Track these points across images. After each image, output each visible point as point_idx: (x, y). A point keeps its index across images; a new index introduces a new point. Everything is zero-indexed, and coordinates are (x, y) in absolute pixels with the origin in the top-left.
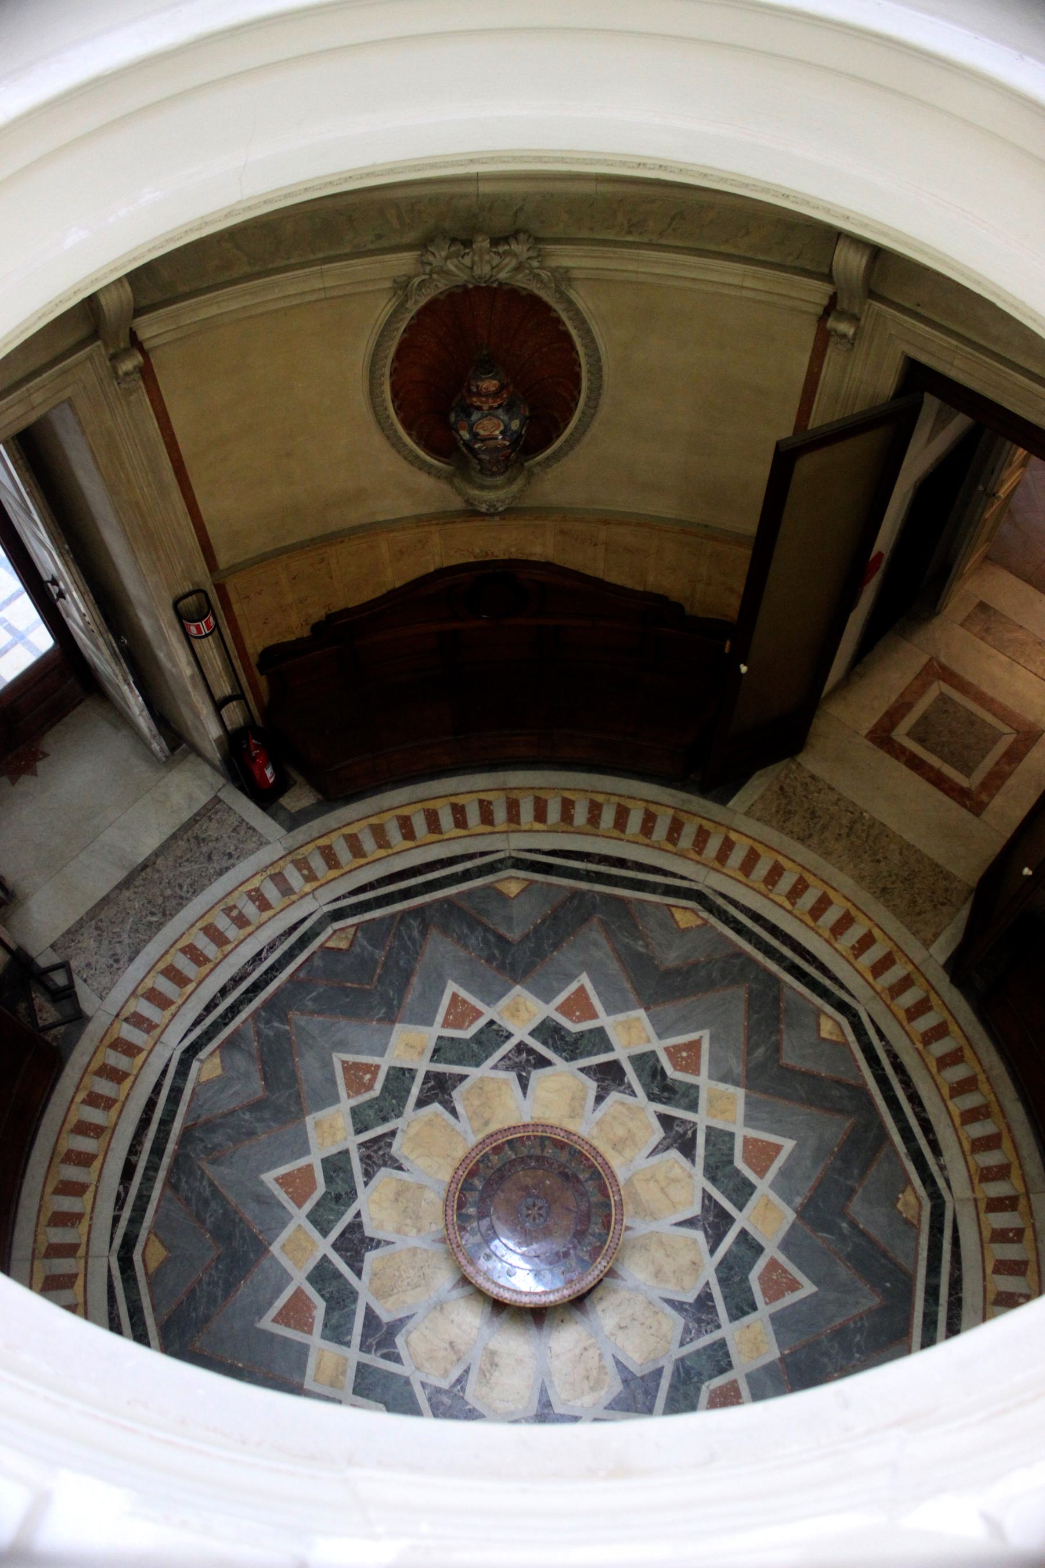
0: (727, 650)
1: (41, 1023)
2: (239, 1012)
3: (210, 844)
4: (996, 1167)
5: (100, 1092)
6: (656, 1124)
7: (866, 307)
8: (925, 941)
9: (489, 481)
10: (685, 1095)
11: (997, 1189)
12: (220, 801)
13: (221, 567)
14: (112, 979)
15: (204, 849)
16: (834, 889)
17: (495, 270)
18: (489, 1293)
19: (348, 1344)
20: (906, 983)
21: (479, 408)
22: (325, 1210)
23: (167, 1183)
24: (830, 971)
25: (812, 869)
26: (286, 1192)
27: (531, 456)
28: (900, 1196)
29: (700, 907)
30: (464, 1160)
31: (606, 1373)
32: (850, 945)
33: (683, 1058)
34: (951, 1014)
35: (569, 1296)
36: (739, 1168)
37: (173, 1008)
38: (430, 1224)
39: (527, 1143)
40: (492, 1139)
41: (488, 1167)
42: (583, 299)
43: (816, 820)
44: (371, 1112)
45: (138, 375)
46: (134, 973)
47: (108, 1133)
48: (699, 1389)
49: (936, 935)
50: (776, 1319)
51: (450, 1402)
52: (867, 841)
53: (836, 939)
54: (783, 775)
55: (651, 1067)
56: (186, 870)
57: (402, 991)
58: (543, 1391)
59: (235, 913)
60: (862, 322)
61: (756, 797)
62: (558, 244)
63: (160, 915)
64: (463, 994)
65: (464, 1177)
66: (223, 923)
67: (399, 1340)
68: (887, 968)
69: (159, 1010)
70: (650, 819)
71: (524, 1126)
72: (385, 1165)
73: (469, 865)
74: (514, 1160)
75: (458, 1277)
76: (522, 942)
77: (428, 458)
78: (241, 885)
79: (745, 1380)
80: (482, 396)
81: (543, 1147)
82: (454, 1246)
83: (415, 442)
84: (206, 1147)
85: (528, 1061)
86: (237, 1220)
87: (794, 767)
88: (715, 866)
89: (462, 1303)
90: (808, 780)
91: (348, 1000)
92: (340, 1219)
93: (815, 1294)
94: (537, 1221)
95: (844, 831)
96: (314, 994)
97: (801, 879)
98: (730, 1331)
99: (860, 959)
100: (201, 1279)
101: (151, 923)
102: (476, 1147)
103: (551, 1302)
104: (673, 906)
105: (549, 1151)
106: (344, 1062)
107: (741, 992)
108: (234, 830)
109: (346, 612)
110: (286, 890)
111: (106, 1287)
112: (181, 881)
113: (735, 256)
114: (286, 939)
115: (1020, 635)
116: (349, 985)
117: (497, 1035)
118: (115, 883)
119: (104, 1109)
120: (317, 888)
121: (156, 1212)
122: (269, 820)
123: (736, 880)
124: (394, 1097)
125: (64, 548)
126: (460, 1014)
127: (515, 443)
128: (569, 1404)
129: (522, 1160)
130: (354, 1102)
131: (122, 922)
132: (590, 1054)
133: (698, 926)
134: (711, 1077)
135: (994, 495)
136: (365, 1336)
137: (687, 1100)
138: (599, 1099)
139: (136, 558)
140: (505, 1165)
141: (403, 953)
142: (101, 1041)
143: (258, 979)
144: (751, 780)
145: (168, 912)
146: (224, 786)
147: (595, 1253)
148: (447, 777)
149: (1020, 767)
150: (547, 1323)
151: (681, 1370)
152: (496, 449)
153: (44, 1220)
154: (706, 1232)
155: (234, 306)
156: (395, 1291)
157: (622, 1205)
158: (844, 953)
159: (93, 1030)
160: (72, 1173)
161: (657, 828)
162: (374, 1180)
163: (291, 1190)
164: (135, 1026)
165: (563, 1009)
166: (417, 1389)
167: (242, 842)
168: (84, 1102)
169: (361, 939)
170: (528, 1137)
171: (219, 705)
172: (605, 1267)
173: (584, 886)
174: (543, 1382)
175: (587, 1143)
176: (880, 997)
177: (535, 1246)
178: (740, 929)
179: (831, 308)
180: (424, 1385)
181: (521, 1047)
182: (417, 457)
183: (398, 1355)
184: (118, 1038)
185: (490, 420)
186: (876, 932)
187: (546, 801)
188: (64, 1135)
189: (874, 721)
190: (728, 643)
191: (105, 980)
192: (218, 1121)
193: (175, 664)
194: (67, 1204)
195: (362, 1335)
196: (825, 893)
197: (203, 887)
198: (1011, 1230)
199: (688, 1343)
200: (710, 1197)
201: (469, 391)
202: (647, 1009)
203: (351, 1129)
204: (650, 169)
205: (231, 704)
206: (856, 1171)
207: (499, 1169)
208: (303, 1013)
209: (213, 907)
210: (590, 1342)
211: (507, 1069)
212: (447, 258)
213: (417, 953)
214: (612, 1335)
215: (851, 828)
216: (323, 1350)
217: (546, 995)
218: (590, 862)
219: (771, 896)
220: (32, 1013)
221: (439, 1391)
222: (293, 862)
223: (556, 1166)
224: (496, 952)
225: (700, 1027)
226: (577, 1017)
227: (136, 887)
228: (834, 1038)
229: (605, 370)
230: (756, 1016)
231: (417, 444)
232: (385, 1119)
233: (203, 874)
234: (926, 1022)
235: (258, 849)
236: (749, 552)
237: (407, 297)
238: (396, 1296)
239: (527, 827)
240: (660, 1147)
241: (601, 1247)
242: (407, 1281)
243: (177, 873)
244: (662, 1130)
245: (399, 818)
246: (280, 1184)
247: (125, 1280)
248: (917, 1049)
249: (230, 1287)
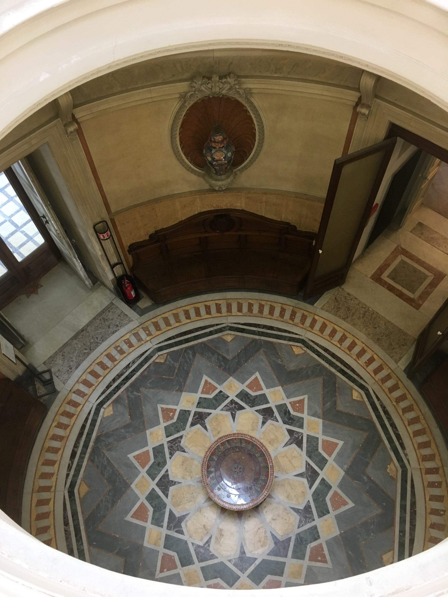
0: (314, 244)
1: (39, 395)
2: (120, 388)
3: (109, 321)
4: (429, 455)
5: (63, 422)
6: (287, 433)
7: (374, 102)
8: (396, 360)
9: (219, 177)
10: (298, 421)
11: (430, 465)
12: (113, 304)
13: (112, 212)
14: (69, 376)
15: (107, 323)
16: (358, 339)
17: (221, 90)
18: (220, 505)
19: (162, 526)
20: (388, 377)
21: (215, 148)
22: (154, 469)
23: (89, 458)
24: (356, 372)
25: (348, 331)
26: (138, 462)
27: (236, 167)
28: (388, 466)
29: (303, 346)
30: (209, 449)
31: (268, 539)
32: (365, 362)
33: (297, 407)
34: (408, 390)
35: (252, 506)
36: (321, 452)
37: (94, 387)
38: (196, 474)
39: (235, 441)
40: (221, 440)
41: (219, 451)
42: (256, 101)
43: (350, 311)
44: (173, 428)
45: (76, 133)
46: (77, 373)
47: (65, 439)
48: (306, 547)
49: (400, 358)
50: (338, 518)
51: (203, 551)
52: (371, 319)
53: (359, 359)
54: (336, 293)
55: (284, 410)
56: (99, 331)
57: (185, 379)
58: (242, 547)
59: (119, 349)
60: (372, 108)
61: (326, 302)
62: (246, 78)
63: (89, 350)
64: (210, 380)
65: (210, 455)
66: (114, 353)
67: (183, 525)
68: (380, 371)
69: (88, 388)
70: (283, 311)
71: (233, 434)
72: (178, 450)
73: (212, 329)
74: (230, 448)
75: (207, 497)
76: (232, 359)
77: (192, 166)
78: (121, 338)
79: (325, 543)
80: (216, 143)
81: (241, 443)
82: (205, 484)
83: (190, 162)
84: (106, 444)
85: (235, 407)
86: (118, 474)
87: (341, 290)
88: (309, 330)
89: (209, 508)
90: (347, 295)
91: (164, 383)
92: (159, 473)
93: (353, 507)
94: (239, 474)
95: (361, 316)
96: (151, 380)
97: (344, 335)
98: (318, 522)
99: (368, 367)
100: (102, 500)
101: (85, 353)
102: (215, 443)
103: (245, 508)
104: (292, 345)
105: (244, 445)
106: (162, 408)
107: (320, 380)
108: (119, 316)
109: (162, 230)
110: (140, 339)
111: (63, 504)
112: (97, 336)
113: (319, 81)
114: (139, 359)
115: (436, 236)
116: (164, 377)
117: (223, 397)
118: (70, 337)
119: (64, 429)
120: (152, 339)
121: (84, 471)
122: (133, 312)
123: (318, 335)
124: (182, 422)
125: (48, 203)
126: (208, 388)
127: (229, 162)
128: (252, 552)
129: (233, 448)
130: (165, 424)
131: (73, 353)
132: (260, 405)
133: (302, 353)
134: (308, 414)
135: (426, 178)
136: (169, 523)
137: (299, 424)
138: (264, 423)
139: (78, 208)
140: (226, 450)
141: (186, 364)
142: (63, 401)
143: (128, 375)
144: (323, 295)
145: (92, 349)
146: (115, 298)
147: (263, 487)
148: (203, 294)
149: (436, 289)
150: (243, 517)
151: (299, 538)
152: (221, 165)
153: (37, 476)
154: (308, 479)
155: (115, 104)
156: (181, 503)
157: (273, 467)
158: (362, 365)
159: (60, 397)
160: (50, 456)
161: (286, 314)
162: (174, 456)
163: (140, 461)
164: (77, 395)
165: (249, 386)
166: (190, 545)
167: (122, 320)
168: (55, 426)
169: (169, 359)
170: (235, 439)
171: (112, 267)
172: (267, 494)
173: (257, 337)
174: (242, 543)
175: (259, 441)
176: (378, 383)
177: (238, 484)
178: (319, 355)
179: (359, 103)
180: (193, 544)
181: (232, 402)
182: (190, 168)
183: (182, 531)
184: (71, 400)
185: (219, 152)
186: (375, 356)
187: (242, 304)
188: (47, 440)
189: (374, 271)
190: (314, 241)
191: (66, 376)
192: (111, 433)
193: (95, 250)
194: (47, 469)
195: (168, 522)
196: (354, 340)
197: (106, 339)
198: (436, 482)
199: (301, 527)
200: (309, 464)
201: (211, 140)
202: (282, 387)
203: (165, 435)
204: (284, 47)
205: (117, 266)
206: (369, 455)
207: (224, 452)
208: (146, 388)
209: (110, 346)
210: (261, 526)
211: (227, 410)
212: (201, 85)
213: (192, 364)
214: (271, 522)
215: (364, 314)
216: (152, 529)
217: (242, 381)
218: (259, 328)
219: (332, 341)
220: (35, 391)
221: (199, 546)
222: (142, 328)
223: (246, 451)
224: (223, 364)
225: (303, 394)
226: (255, 390)
227: (79, 339)
228: (358, 399)
229: (265, 131)
230: (326, 390)
231: (190, 162)
232: (178, 431)
233: (106, 333)
234: (397, 394)
235: (128, 323)
236: (323, 205)
237: (185, 102)
238: (182, 506)
239: (235, 314)
240: (288, 443)
241: (265, 485)
242: (186, 499)
243: (96, 333)
244: (289, 436)
245: (184, 310)
246: (136, 459)
247: (70, 501)
248: (393, 405)
249: (114, 503)
